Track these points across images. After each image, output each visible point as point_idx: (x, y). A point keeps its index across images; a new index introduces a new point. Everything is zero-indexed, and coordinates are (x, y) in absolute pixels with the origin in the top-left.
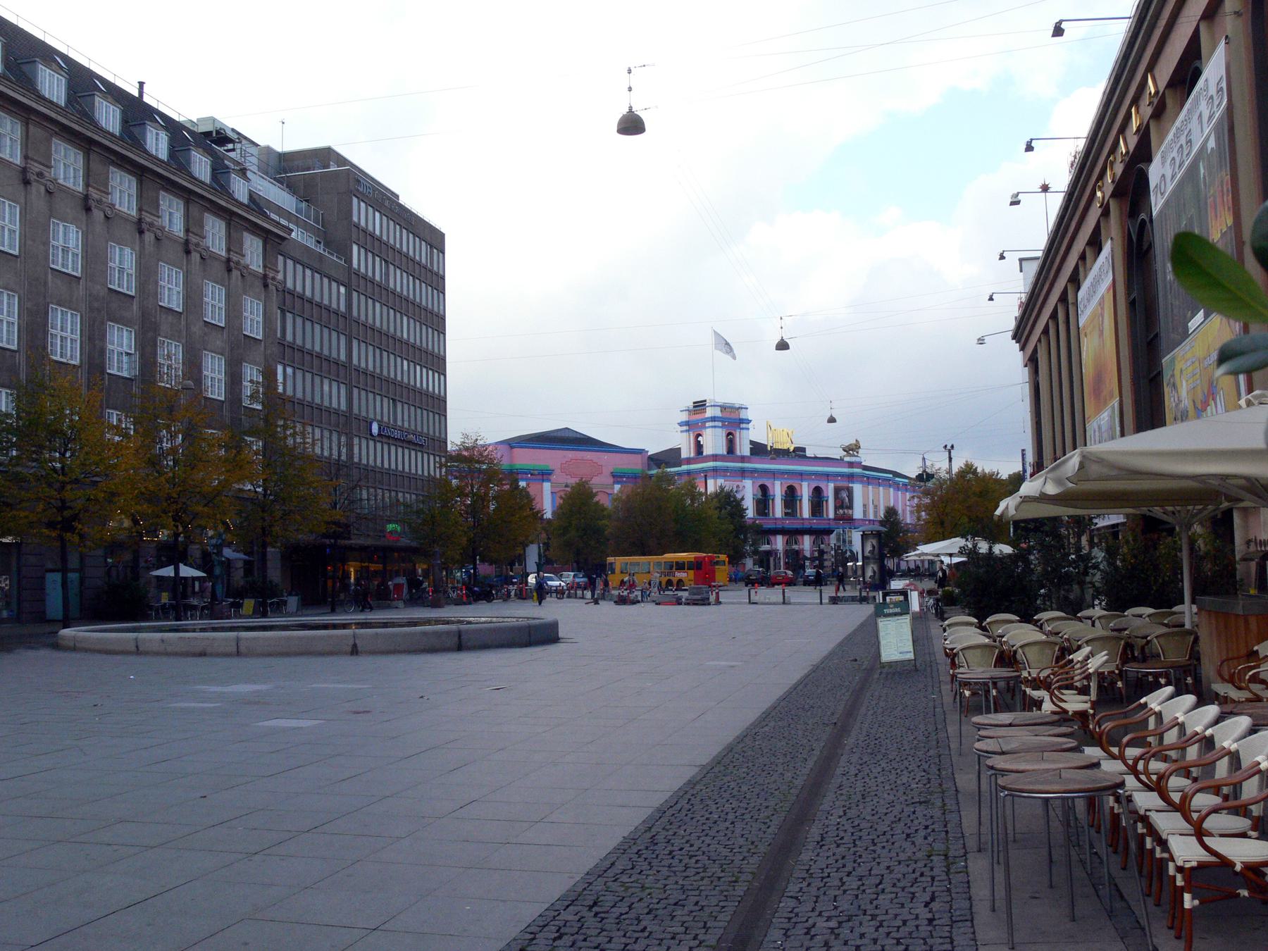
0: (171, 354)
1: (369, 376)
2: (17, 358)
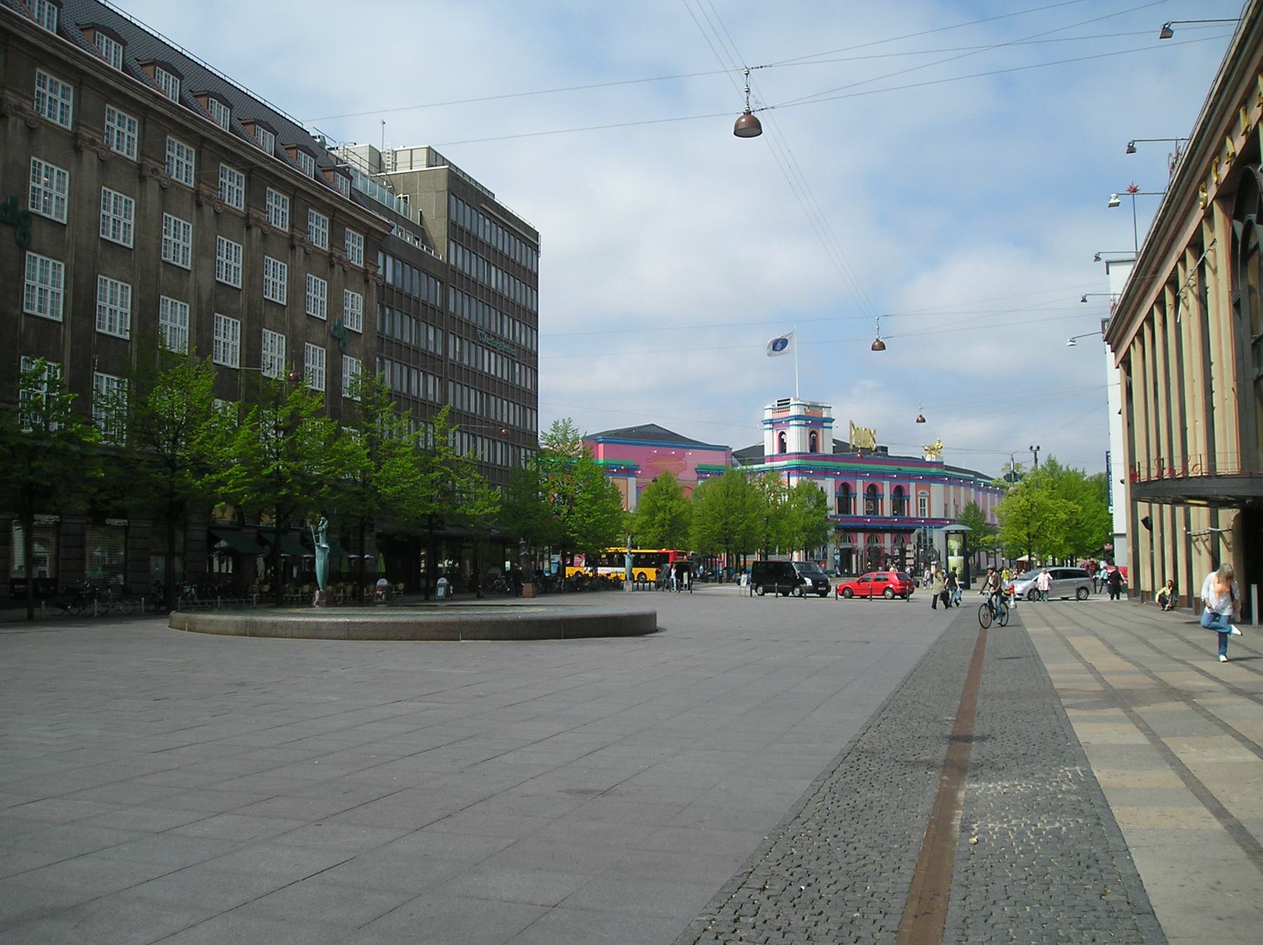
0: (274, 348)
1: (420, 355)
2: (129, 347)
